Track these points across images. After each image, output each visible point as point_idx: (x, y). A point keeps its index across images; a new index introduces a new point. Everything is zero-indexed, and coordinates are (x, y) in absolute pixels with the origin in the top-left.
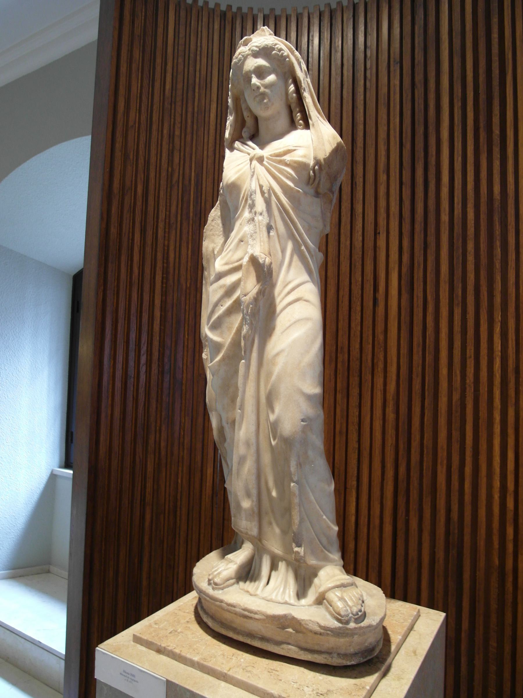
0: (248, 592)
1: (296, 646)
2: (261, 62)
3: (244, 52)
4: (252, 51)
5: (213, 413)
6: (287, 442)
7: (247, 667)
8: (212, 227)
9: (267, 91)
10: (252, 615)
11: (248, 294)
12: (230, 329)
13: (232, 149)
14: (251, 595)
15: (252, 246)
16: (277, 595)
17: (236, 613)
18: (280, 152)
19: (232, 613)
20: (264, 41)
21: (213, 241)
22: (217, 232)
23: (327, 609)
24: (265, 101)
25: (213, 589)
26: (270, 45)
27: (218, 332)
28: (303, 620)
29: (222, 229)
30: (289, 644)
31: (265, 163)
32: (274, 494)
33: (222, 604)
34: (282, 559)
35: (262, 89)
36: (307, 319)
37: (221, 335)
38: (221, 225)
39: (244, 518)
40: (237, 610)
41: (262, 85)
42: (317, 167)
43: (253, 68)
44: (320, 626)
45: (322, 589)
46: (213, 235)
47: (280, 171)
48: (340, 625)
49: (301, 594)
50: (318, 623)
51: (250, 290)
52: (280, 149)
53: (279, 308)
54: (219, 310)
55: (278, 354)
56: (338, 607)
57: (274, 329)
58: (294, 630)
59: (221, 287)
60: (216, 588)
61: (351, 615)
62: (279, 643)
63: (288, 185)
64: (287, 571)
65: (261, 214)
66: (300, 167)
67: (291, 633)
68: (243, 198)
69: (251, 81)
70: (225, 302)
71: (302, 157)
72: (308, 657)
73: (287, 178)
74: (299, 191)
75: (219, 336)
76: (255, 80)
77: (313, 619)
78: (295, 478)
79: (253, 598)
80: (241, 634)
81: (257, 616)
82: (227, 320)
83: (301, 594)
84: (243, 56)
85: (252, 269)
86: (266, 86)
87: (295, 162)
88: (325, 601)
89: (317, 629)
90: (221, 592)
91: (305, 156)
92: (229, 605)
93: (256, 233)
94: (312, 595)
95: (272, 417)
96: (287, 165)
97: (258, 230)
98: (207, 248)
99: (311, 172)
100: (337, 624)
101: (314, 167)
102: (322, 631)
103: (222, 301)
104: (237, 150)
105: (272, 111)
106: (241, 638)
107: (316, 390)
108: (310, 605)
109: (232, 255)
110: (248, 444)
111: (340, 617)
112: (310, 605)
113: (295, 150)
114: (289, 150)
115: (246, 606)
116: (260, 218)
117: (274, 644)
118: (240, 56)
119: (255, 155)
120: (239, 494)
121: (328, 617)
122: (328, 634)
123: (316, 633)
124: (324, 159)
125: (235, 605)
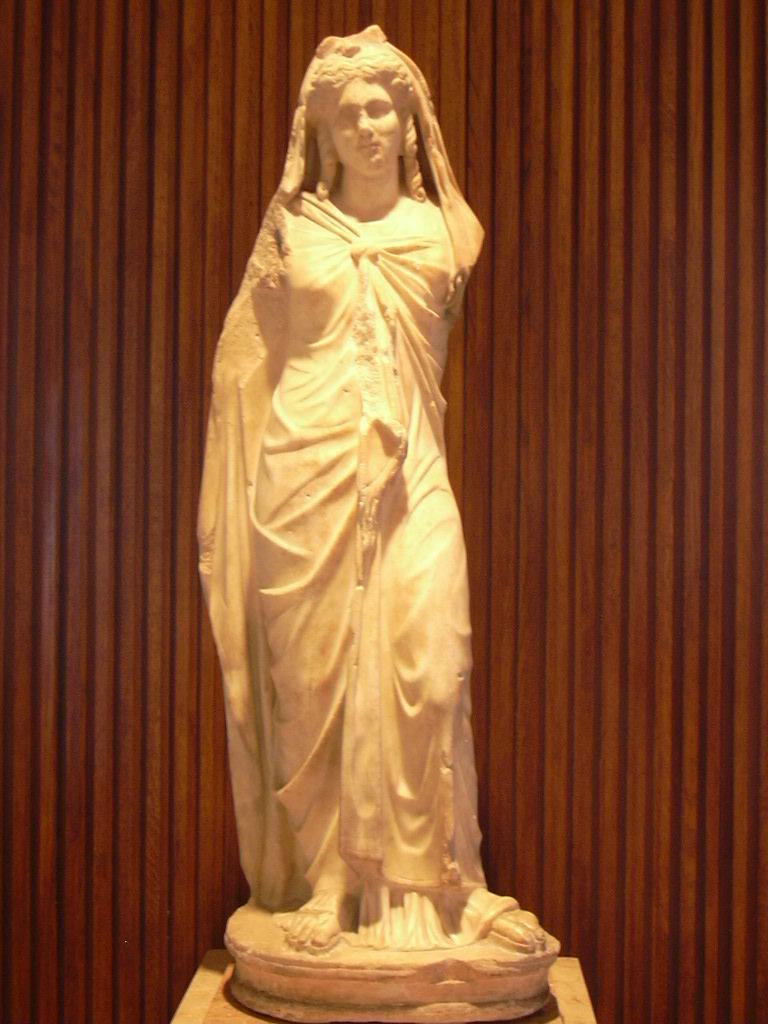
0: (371, 946)
2: (379, 93)
6: (435, 710)
10: (395, 973)
11: (371, 482)
14: (376, 949)
15: (373, 404)
23: (498, 941)
25: (313, 953)
28: (473, 962)
31: (380, 262)
34: (410, 889)
36: (438, 457)
37: (307, 543)
40: (368, 972)
44: (499, 964)
47: (405, 280)
48: (526, 956)
53: (413, 499)
55: (418, 578)
58: (461, 980)
59: (306, 465)
61: (536, 941)
65: (386, 353)
66: (438, 280)
68: (342, 316)
73: (417, 292)
74: (431, 315)
77: (486, 958)
81: (402, 973)
84: (347, 75)
87: (430, 269)
88: (492, 933)
89: (495, 968)
90: (327, 955)
93: (377, 383)
95: (408, 675)
100: (519, 956)
101: (456, 278)
102: (502, 969)
105: (371, 171)
111: (524, 946)
119: (366, 249)
120: (354, 798)
123: (493, 975)
124: (471, 267)
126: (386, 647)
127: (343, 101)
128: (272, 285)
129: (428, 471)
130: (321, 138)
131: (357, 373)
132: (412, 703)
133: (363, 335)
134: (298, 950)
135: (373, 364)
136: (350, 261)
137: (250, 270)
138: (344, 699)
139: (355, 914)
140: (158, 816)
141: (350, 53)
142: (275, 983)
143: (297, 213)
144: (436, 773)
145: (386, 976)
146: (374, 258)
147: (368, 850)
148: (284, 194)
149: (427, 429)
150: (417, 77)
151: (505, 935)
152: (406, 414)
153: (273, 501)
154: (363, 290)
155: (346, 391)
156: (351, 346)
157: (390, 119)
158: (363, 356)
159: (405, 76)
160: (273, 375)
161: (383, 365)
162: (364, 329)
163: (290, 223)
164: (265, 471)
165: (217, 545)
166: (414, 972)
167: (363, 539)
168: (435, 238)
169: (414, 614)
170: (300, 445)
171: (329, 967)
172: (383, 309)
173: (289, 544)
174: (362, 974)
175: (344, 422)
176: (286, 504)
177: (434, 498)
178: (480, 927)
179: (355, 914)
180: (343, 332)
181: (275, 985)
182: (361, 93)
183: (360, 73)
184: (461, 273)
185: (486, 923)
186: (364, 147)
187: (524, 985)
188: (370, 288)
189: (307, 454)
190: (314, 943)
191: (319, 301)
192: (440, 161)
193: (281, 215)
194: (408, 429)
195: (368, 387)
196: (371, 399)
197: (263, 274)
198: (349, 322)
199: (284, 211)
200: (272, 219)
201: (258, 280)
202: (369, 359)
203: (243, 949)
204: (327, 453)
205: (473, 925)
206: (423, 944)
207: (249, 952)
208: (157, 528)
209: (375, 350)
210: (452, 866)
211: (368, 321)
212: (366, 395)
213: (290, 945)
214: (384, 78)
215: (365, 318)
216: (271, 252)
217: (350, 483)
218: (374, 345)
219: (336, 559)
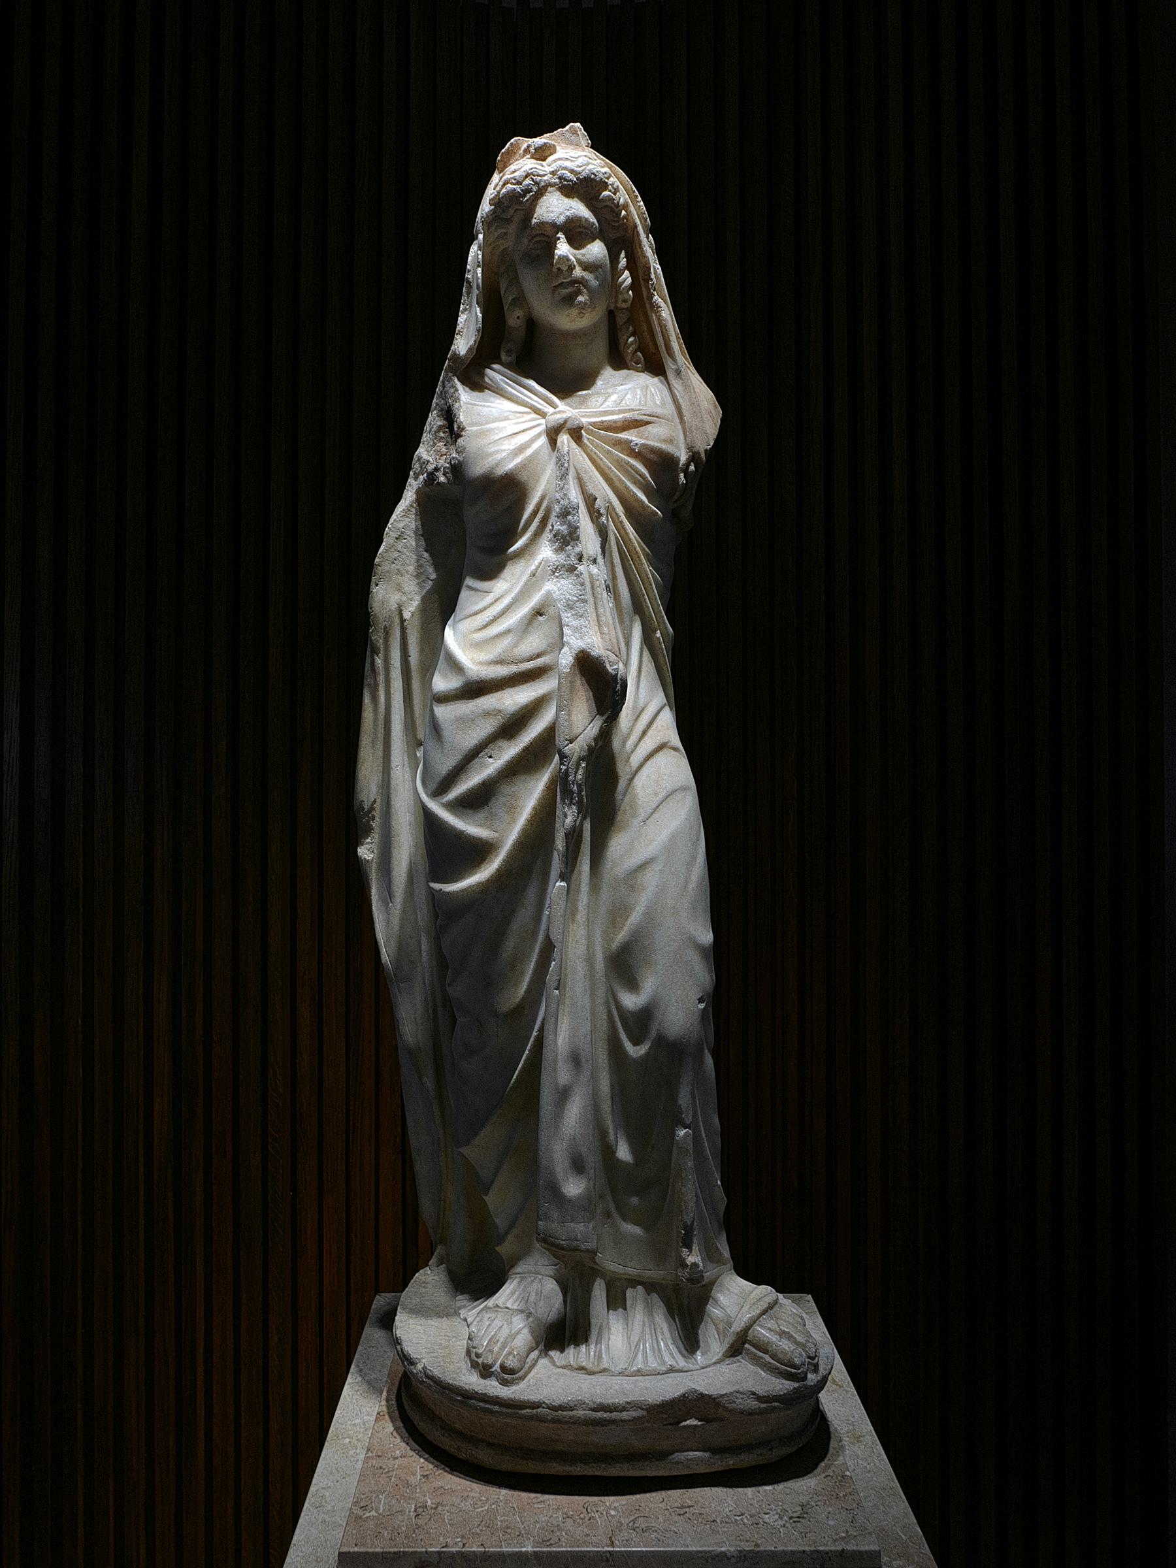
0: (582, 1368)
4: (560, 178)
6: (671, 1052)
7: (634, 1521)
8: (396, 555)
9: (588, 276)
10: (615, 1415)
12: (512, 810)
13: (476, 384)
14: (591, 1373)
15: (576, 629)
16: (646, 1359)
17: (576, 1422)
20: (588, 164)
23: (757, 1361)
25: (505, 1383)
26: (601, 175)
27: (482, 814)
32: (624, 1152)
34: (633, 1283)
35: (578, 272)
36: (684, 789)
40: (580, 1413)
41: (580, 262)
42: (692, 467)
43: (562, 218)
44: (759, 1398)
45: (738, 1326)
48: (796, 1385)
49: (690, 1342)
50: (753, 1393)
51: (580, 730)
54: (486, 766)
55: (642, 867)
56: (784, 1352)
59: (487, 714)
60: (513, 1379)
62: (663, 1455)
63: (638, 499)
65: (595, 561)
68: (535, 513)
69: (555, 247)
70: (501, 749)
71: (665, 441)
73: (635, 483)
76: (563, 248)
78: (688, 1119)
81: (625, 1415)
83: (690, 1342)
84: (536, 183)
85: (579, 682)
86: (586, 267)
87: (653, 450)
88: (747, 1346)
89: (754, 1404)
91: (670, 441)
92: (554, 1408)
94: (713, 1344)
95: (630, 1001)
97: (589, 597)
99: (682, 475)
100: (790, 1385)
101: (688, 465)
107: (706, 937)
108: (719, 1362)
110: (575, 1060)
112: (719, 1362)
113: (648, 423)
114: (636, 420)
116: (594, 570)
118: (528, 181)
119: (565, 422)
122: (774, 1408)
125: (572, 1404)
126: (600, 964)
129: (650, 721)
131: (558, 588)
132: (636, 1043)
133: (563, 537)
137: (416, 466)
138: (541, 1030)
141: (542, 154)
148: (456, 358)
149: (649, 667)
150: (635, 202)
151: (766, 1352)
152: (623, 648)
154: (563, 476)
156: (546, 552)
157: (596, 250)
159: (616, 191)
160: (443, 605)
161: (591, 575)
162: (564, 529)
163: (466, 401)
164: (436, 729)
165: (376, 824)
166: (644, 1413)
167: (565, 816)
168: (660, 411)
170: (475, 689)
171: (527, 1407)
172: (590, 500)
173: (470, 827)
177: (661, 759)
178: (730, 1339)
182: (556, 207)
184: (694, 457)
188: (572, 473)
189: (488, 702)
191: (506, 492)
193: (453, 387)
194: (626, 664)
195: (570, 607)
196: (574, 623)
197: (430, 468)
198: (545, 520)
199: (459, 385)
200: (444, 395)
202: (572, 569)
204: (521, 696)
205: (722, 1334)
206: (653, 1364)
210: (690, 1259)
211: (570, 517)
212: (567, 617)
213: (474, 1365)
214: (584, 188)
215: (565, 513)
217: (545, 747)
218: (577, 549)
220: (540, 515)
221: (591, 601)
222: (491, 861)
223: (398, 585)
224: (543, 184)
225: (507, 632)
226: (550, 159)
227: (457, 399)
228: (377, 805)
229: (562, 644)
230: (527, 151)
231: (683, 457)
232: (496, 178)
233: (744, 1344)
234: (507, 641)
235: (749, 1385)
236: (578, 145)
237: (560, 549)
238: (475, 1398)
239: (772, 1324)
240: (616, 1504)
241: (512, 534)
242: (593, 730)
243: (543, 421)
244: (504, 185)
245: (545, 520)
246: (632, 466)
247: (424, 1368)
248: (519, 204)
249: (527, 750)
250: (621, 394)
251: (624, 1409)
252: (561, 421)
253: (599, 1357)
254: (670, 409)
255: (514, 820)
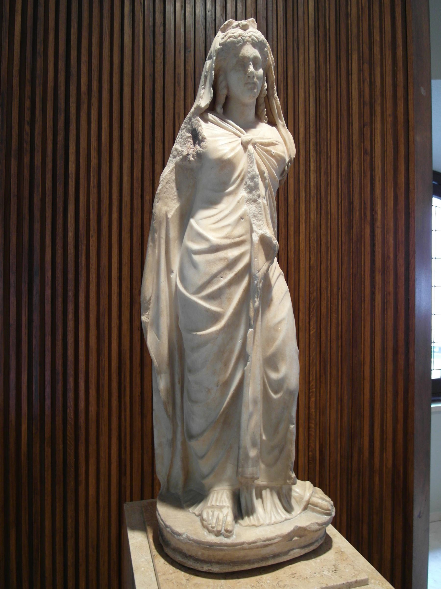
0: (253, 525)
1: (298, 548)
3: (244, 36)
4: (252, 39)
5: (163, 375)
8: (166, 190)
9: (258, 82)
10: (272, 542)
12: (230, 300)
15: (259, 226)
17: (258, 547)
18: (265, 143)
19: (255, 548)
21: (166, 204)
22: (171, 196)
23: (313, 510)
24: (255, 91)
25: (227, 537)
27: (217, 302)
28: (307, 526)
29: (176, 194)
30: (293, 549)
32: (264, 438)
33: (244, 545)
34: (265, 487)
37: (220, 305)
38: (175, 189)
39: (250, 465)
40: (259, 544)
42: (290, 164)
43: (252, 56)
46: (167, 197)
52: (263, 139)
53: (273, 282)
55: (280, 322)
57: (271, 300)
58: (298, 537)
59: (221, 259)
64: (272, 495)
67: (297, 540)
68: (239, 176)
70: (226, 274)
72: (307, 550)
73: (273, 168)
75: (217, 306)
76: (251, 68)
79: (260, 529)
80: (256, 562)
81: (275, 541)
82: (228, 291)
83: (288, 508)
84: (243, 40)
87: (280, 156)
88: (309, 505)
89: (317, 527)
92: (249, 543)
95: (274, 376)
96: (272, 155)
97: (263, 212)
98: (160, 210)
99: (287, 167)
103: (222, 273)
104: (211, 122)
106: (256, 566)
109: (232, 231)
112: (300, 513)
113: (277, 144)
114: (273, 143)
115: (266, 537)
117: (284, 556)
119: (251, 140)
121: (318, 515)
123: (316, 531)
127: (240, 55)
128: (192, 159)
130: (221, 78)
132: (276, 392)
134: (217, 535)
135: (258, 204)
136: (241, 147)
137: (174, 152)
139: (241, 510)
140: (72, 417)
142: (199, 553)
143: (206, 121)
144: (288, 428)
145: (267, 543)
146: (254, 145)
147: (253, 474)
153: (198, 279)
155: (242, 219)
156: (243, 193)
157: (261, 72)
158: (251, 199)
160: (185, 215)
162: (252, 184)
164: (195, 265)
166: (281, 539)
169: (278, 343)
170: (216, 249)
174: (256, 546)
175: (241, 236)
176: (209, 282)
179: (241, 510)
180: (239, 186)
181: (200, 553)
183: (250, 40)
185: (307, 501)
186: (249, 83)
187: (321, 533)
188: (255, 162)
189: (221, 254)
190: (227, 531)
191: (226, 166)
192: (277, 102)
195: (255, 216)
198: (242, 180)
201: (181, 157)
202: (255, 201)
203: (179, 535)
204: (233, 253)
206: (279, 519)
207: (184, 536)
208: (71, 294)
209: (259, 196)
211: (255, 179)
212: (254, 221)
216: (189, 142)
218: (258, 193)
219: (237, 314)
220: (241, 178)
221: (264, 215)
222: (220, 321)
223: (167, 204)
224: (245, 40)
225: (229, 225)
226: (248, 31)
227: (200, 126)
228: (153, 299)
229: (252, 231)
230: (237, 26)
231: (287, 160)
232: (220, 34)
233: (308, 505)
234: (229, 229)
235: (315, 521)
236: (254, 27)
237: (250, 192)
238: (216, 546)
239: (317, 495)
240: (268, 578)
241: (226, 184)
242: (265, 267)
243: (240, 139)
244: (229, 38)
245: (242, 180)
246: (272, 161)
247: (187, 536)
248: (232, 48)
249: (236, 275)
250: (264, 132)
251: (275, 538)
252: (250, 140)
253: (258, 519)
254: (281, 140)
255: (230, 303)
